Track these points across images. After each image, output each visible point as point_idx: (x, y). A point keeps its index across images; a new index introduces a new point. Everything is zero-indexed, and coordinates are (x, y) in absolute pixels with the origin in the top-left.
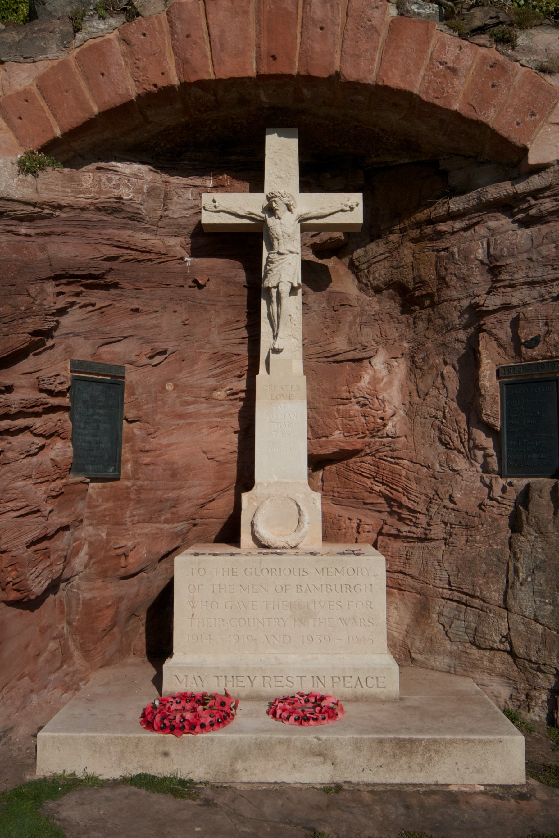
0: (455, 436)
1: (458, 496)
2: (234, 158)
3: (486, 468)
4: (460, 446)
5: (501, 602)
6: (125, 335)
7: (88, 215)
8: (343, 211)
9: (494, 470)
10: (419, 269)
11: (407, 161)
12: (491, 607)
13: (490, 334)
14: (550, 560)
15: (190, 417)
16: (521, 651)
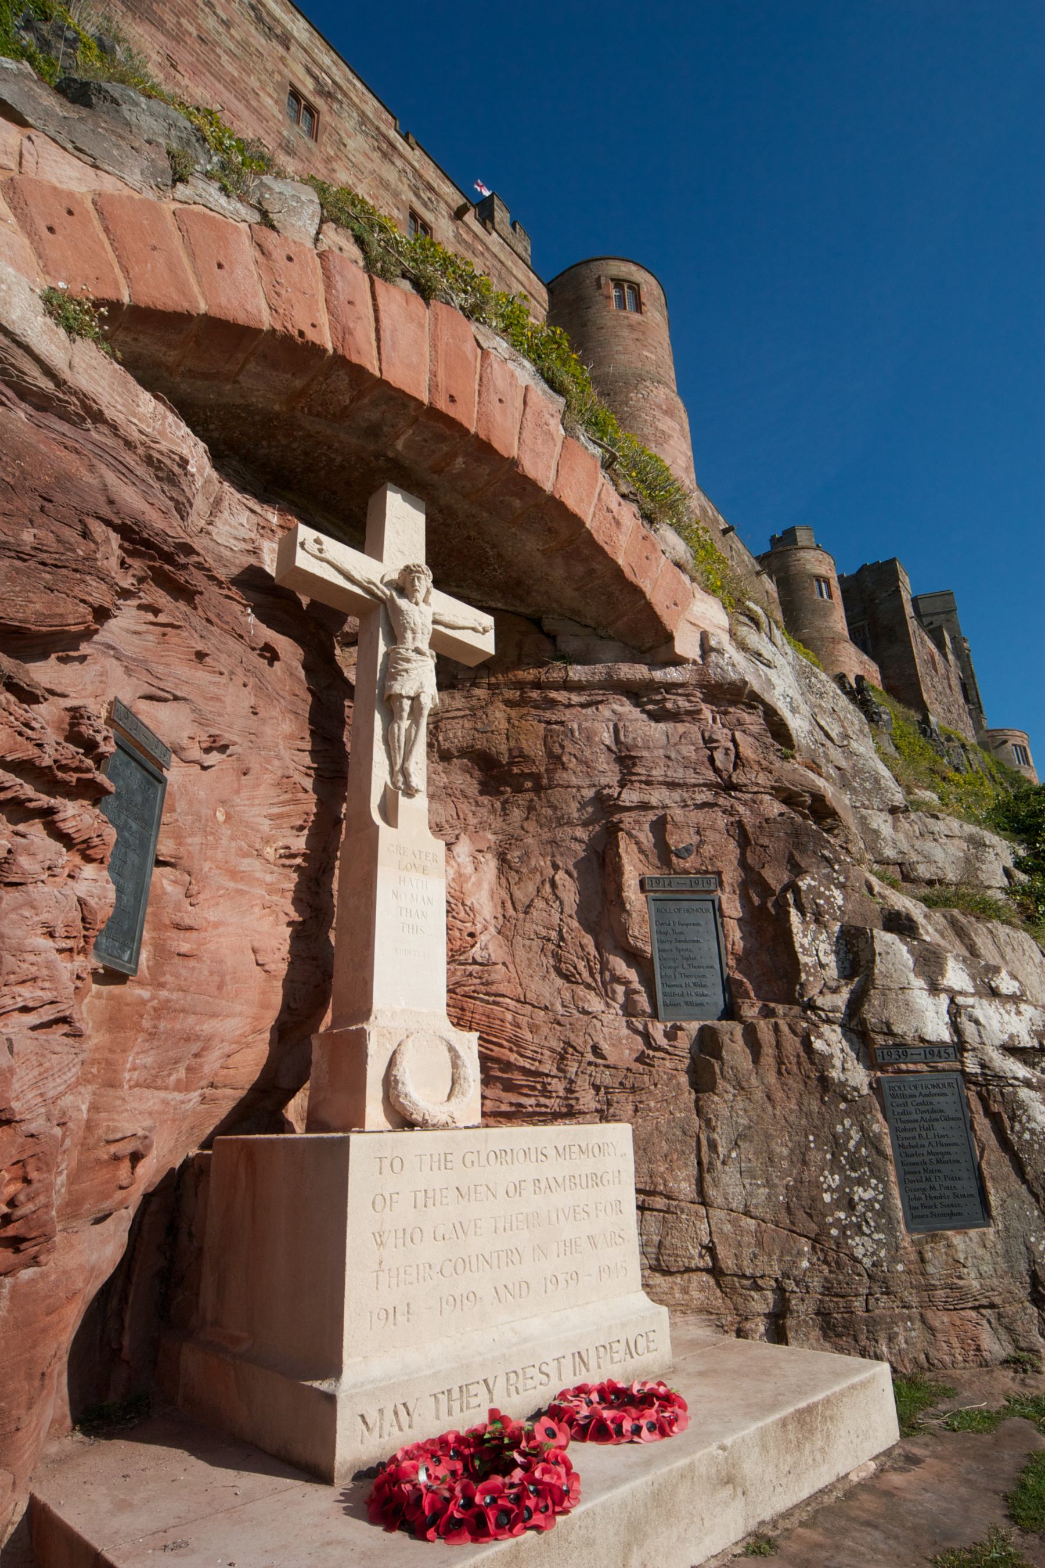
0: (581, 965)
3: (629, 1010)
4: (590, 980)
5: (694, 1195)
6: (179, 694)
7: (129, 458)
8: (474, 629)
9: (644, 1012)
10: (517, 740)
12: (682, 1204)
14: (757, 1124)
15: (242, 879)
16: (728, 1263)
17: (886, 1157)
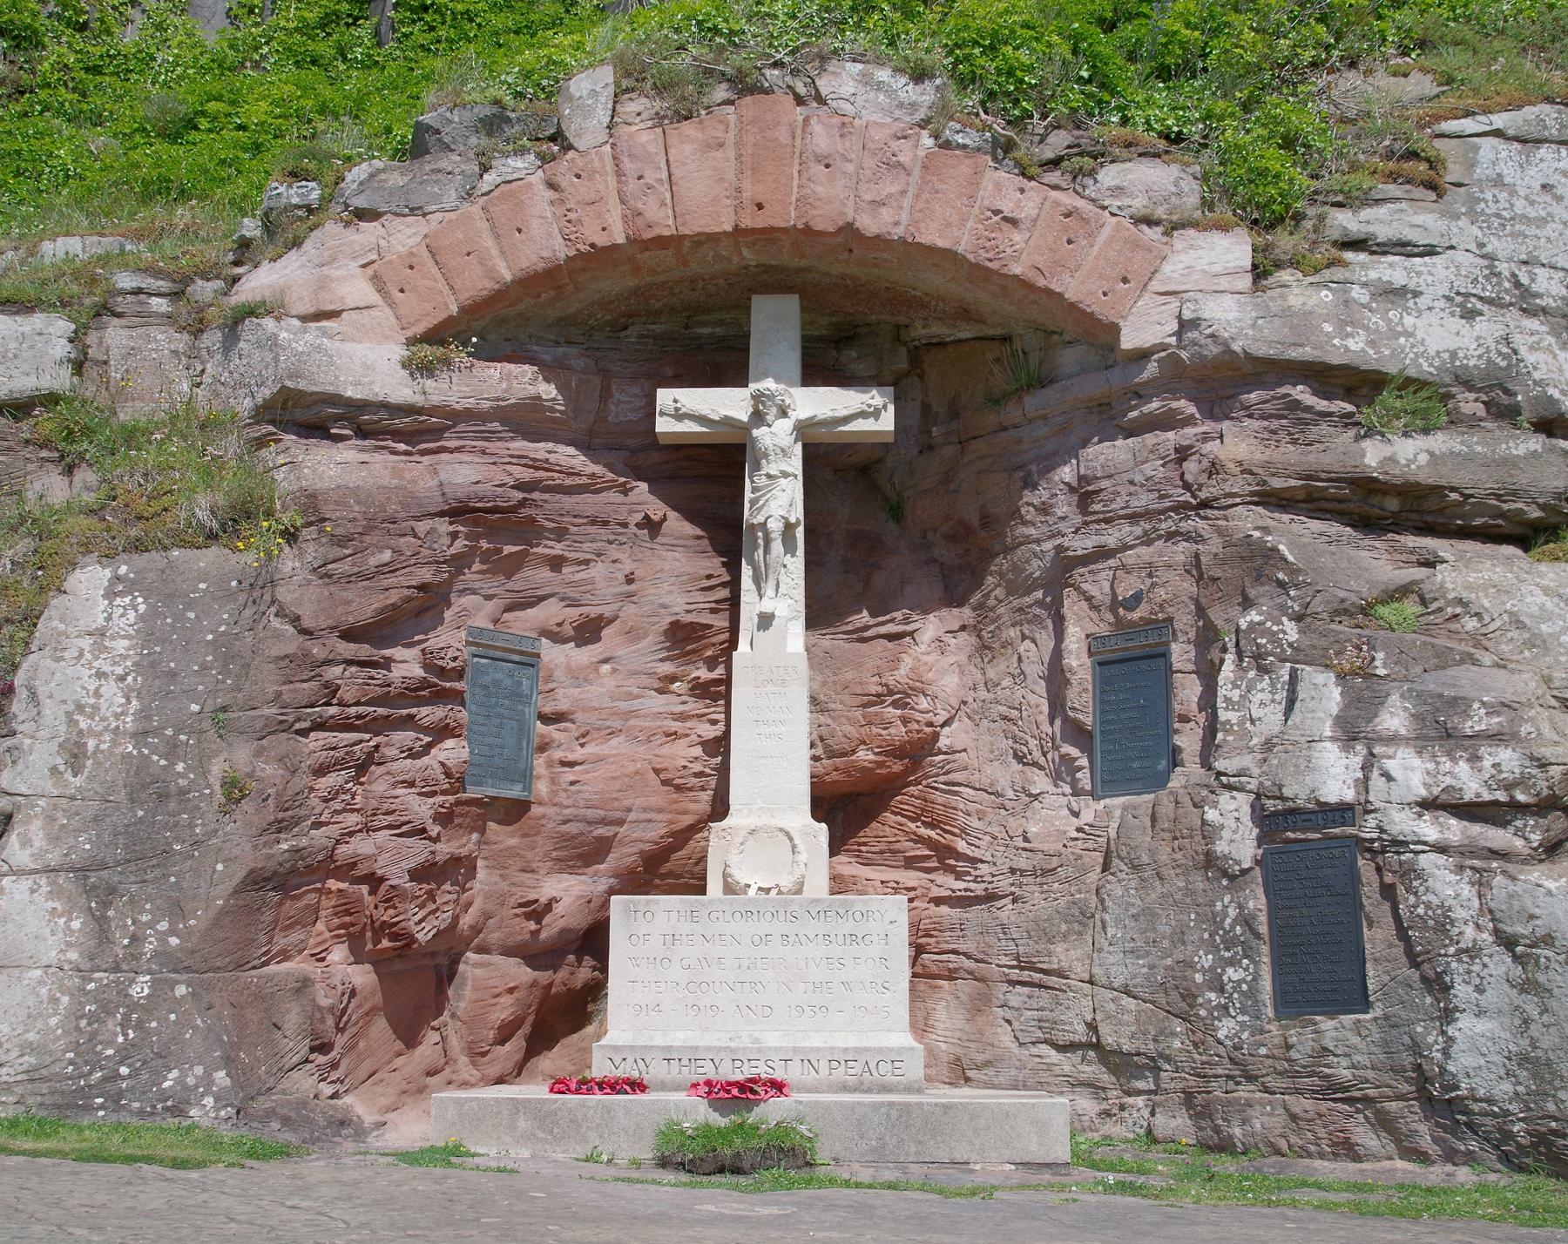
0: (1033, 743)
2: (706, 331)
17: (1258, 936)
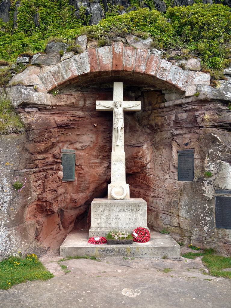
1: (166, 185)
11: (153, 90)
13: (175, 141)
17: (213, 213)
